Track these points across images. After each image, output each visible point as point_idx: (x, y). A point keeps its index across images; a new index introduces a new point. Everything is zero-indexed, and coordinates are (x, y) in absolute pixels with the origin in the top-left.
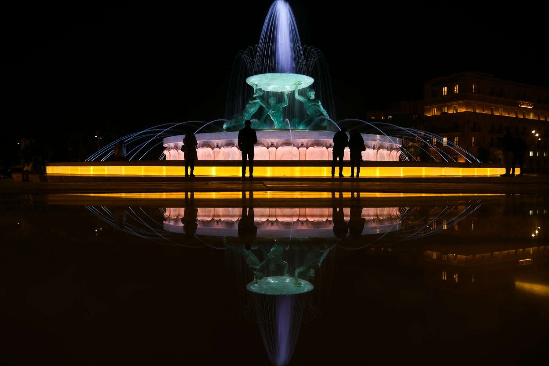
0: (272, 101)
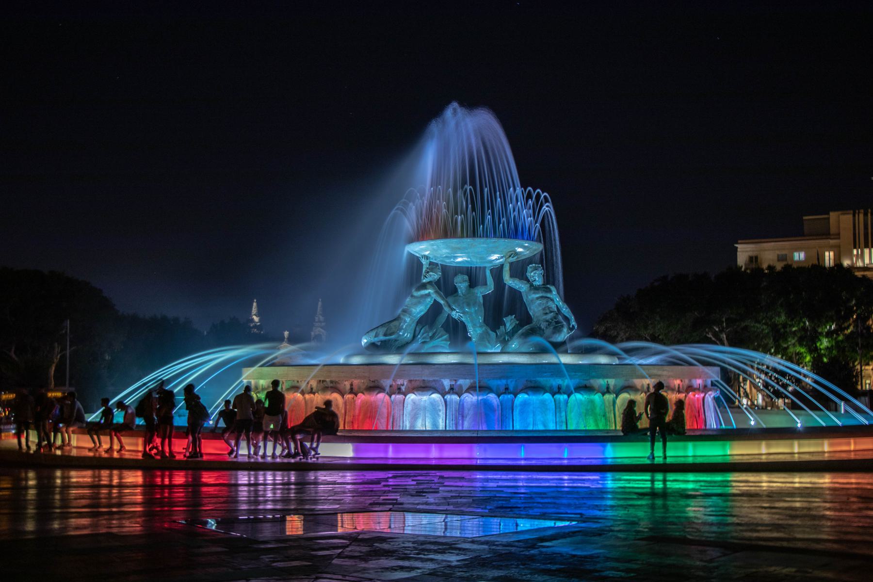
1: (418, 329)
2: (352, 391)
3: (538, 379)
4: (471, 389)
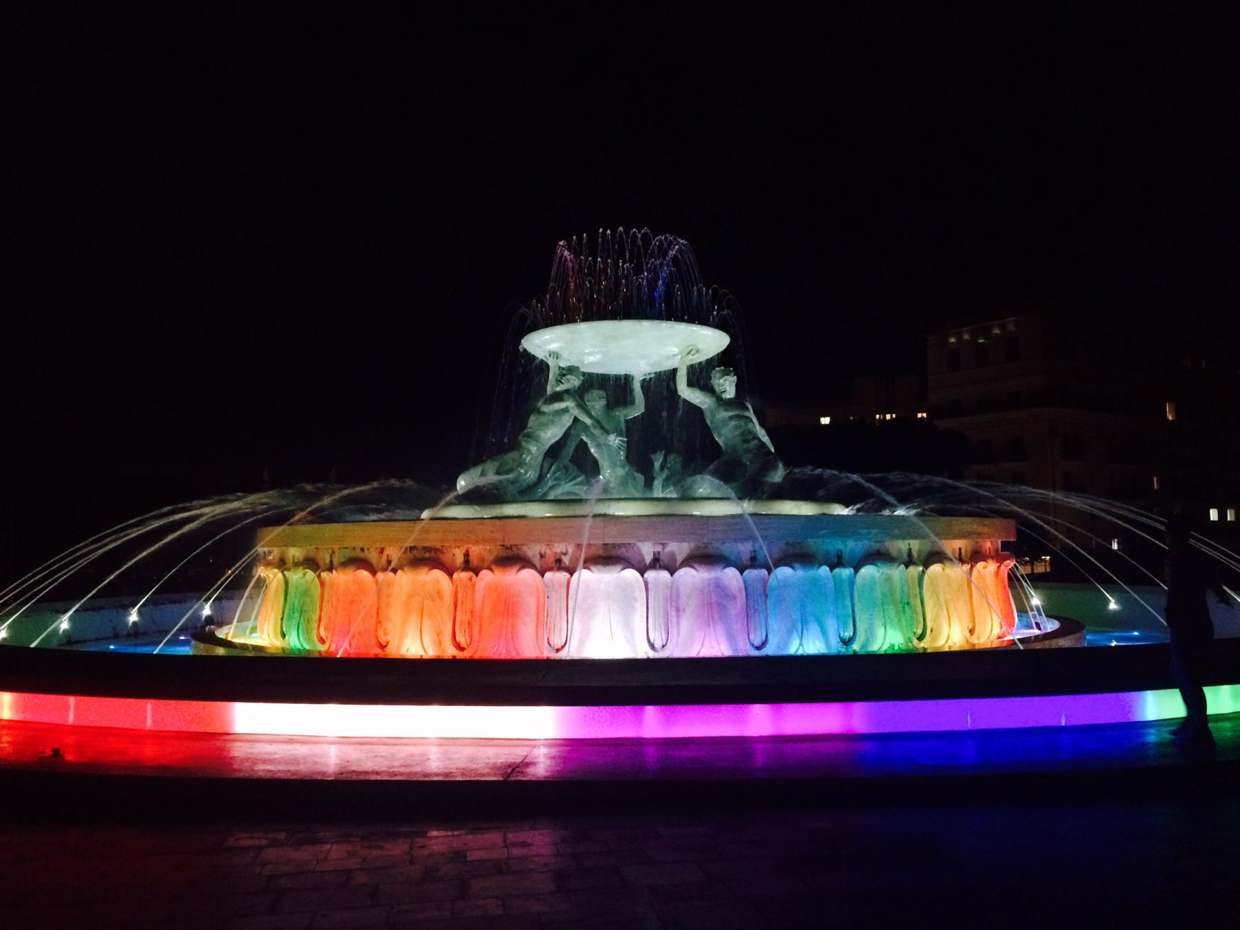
0: (597, 402)
1: (546, 465)
2: (467, 566)
3: (810, 541)
4: (693, 559)
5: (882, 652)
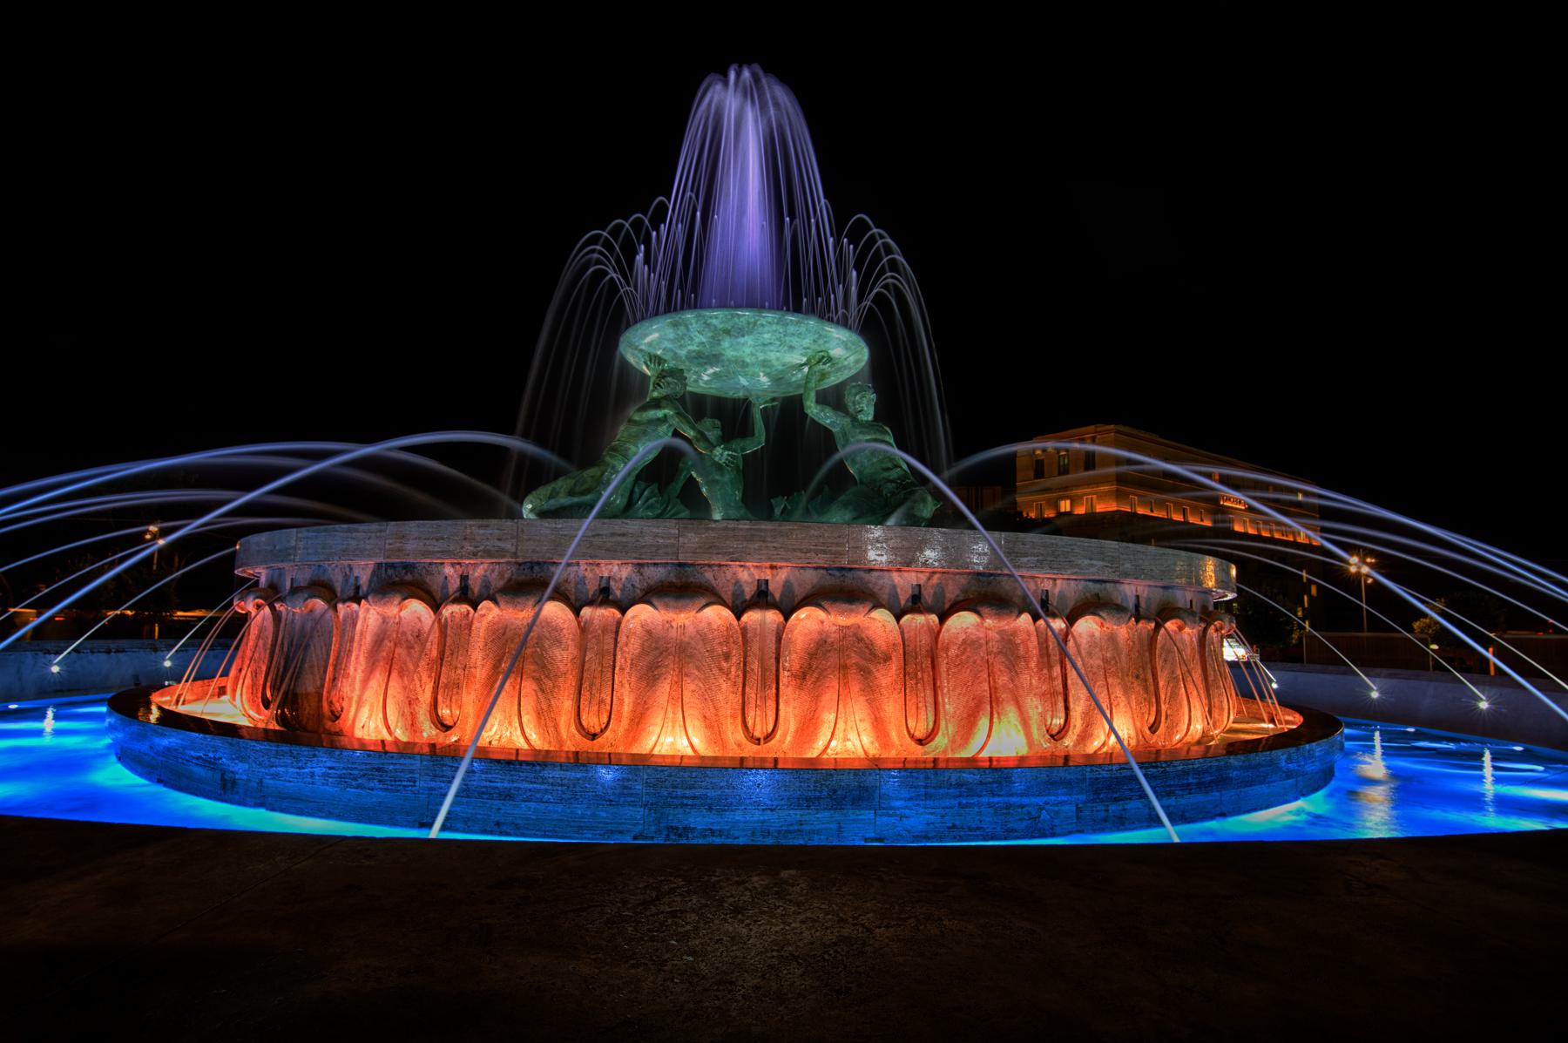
5: (650, 755)
